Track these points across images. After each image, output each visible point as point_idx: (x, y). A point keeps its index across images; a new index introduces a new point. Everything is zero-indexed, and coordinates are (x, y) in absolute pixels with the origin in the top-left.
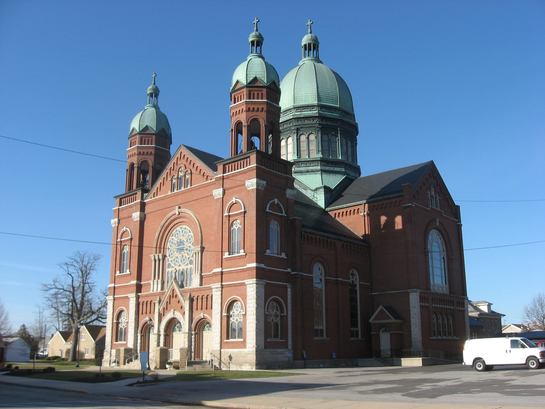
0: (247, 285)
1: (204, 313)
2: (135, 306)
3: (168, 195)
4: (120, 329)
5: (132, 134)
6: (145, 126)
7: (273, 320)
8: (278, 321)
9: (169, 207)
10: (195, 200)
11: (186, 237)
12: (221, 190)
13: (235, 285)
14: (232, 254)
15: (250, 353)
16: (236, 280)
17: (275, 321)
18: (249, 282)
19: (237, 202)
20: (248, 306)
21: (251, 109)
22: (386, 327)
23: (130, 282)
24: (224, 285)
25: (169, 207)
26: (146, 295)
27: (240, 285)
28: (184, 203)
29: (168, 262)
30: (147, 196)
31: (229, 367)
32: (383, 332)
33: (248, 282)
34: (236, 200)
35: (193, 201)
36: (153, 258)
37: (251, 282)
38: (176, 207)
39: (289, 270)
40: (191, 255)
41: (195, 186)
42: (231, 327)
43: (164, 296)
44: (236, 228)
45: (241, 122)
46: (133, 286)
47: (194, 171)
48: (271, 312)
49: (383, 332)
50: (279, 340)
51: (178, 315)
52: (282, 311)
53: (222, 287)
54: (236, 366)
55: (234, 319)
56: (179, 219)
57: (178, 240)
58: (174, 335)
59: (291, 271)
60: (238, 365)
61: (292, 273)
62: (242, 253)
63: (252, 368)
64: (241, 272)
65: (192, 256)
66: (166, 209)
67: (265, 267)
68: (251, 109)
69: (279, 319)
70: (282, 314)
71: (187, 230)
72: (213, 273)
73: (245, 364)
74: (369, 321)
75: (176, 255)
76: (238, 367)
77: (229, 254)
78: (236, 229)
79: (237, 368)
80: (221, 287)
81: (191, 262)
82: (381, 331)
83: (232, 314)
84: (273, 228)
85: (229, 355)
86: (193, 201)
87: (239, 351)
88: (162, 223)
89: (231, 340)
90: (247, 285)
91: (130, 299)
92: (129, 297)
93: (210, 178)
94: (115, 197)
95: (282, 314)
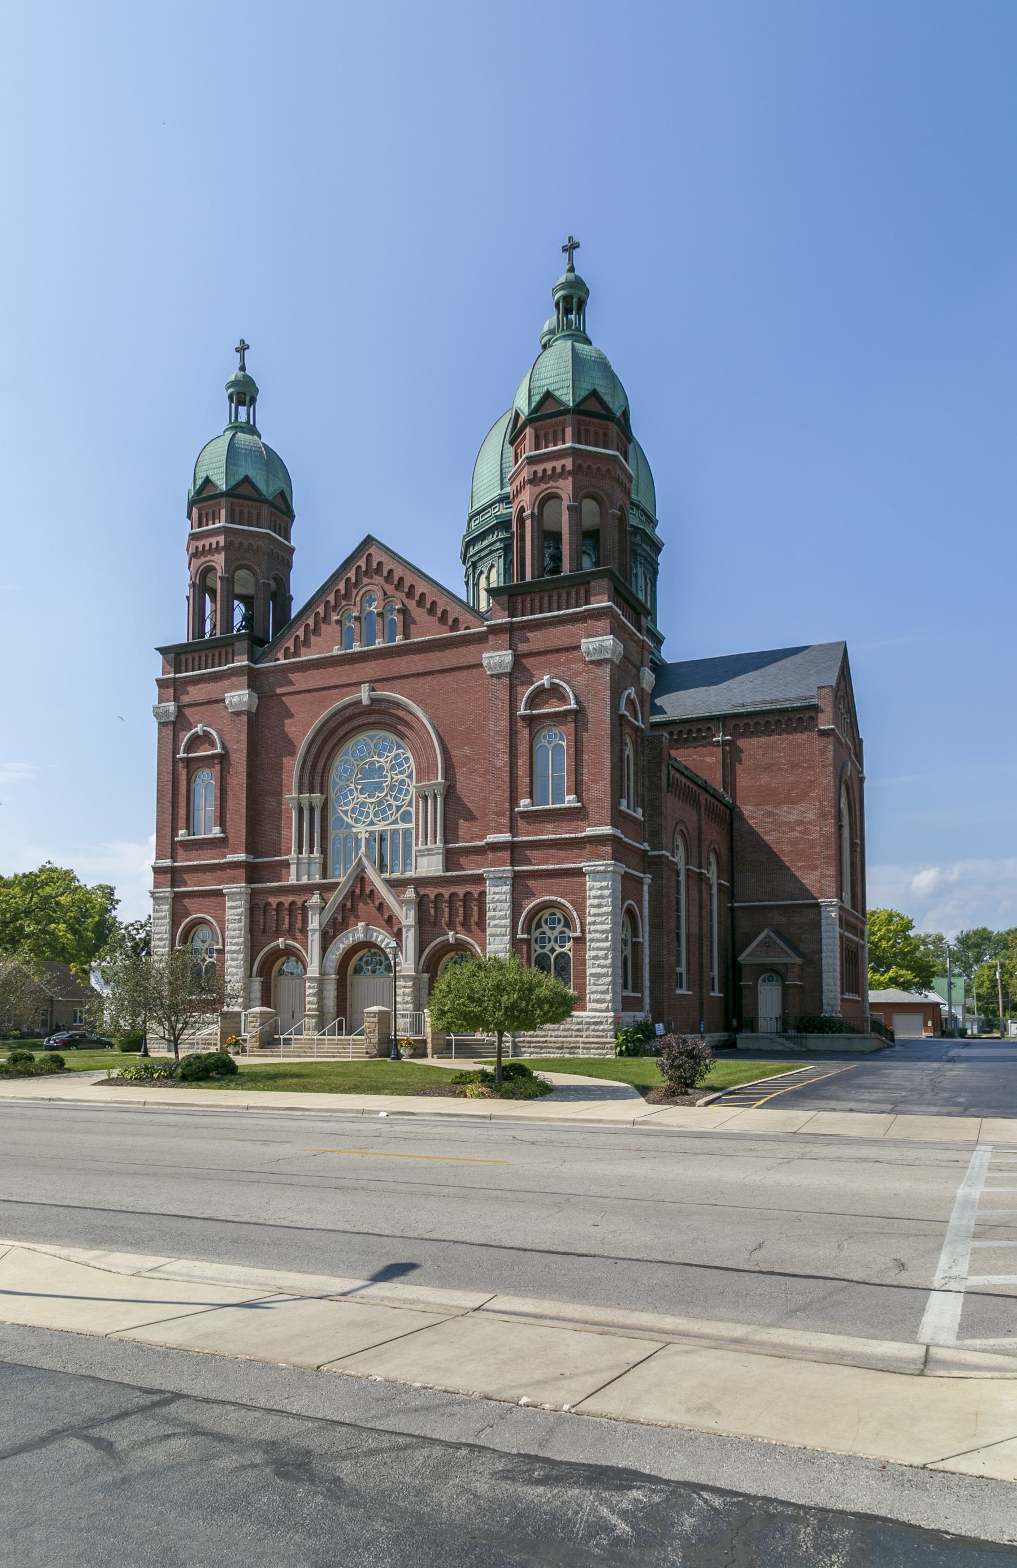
1: (457, 933)
6: (241, 477)
8: (570, 950)
11: (389, 759)
12: (506, 657)
14: (194, 835)
17: (559, 950)
19: (554, 686)
22: (776, 972)
32: (764, 981)
34: (205, 728)
39: (646, 846)
40: (407, 801)
41: (416, 640)
47: (411, 605)
48: (549, 933)
49: (764, 981)
51: (383, 939)
59: (648, 848)
61: (650, 853)
62: (216, 832)
65: (410, 805)
67: (622, 836)
70: (634, 940)
71: (392, 742)
72: (487, 844)
74: (739, 959)
75: (358, 798)
81: (406, 817)
82: (760, 980)
84: (548, 745)
93: (464, 626)
95: (634, 940)
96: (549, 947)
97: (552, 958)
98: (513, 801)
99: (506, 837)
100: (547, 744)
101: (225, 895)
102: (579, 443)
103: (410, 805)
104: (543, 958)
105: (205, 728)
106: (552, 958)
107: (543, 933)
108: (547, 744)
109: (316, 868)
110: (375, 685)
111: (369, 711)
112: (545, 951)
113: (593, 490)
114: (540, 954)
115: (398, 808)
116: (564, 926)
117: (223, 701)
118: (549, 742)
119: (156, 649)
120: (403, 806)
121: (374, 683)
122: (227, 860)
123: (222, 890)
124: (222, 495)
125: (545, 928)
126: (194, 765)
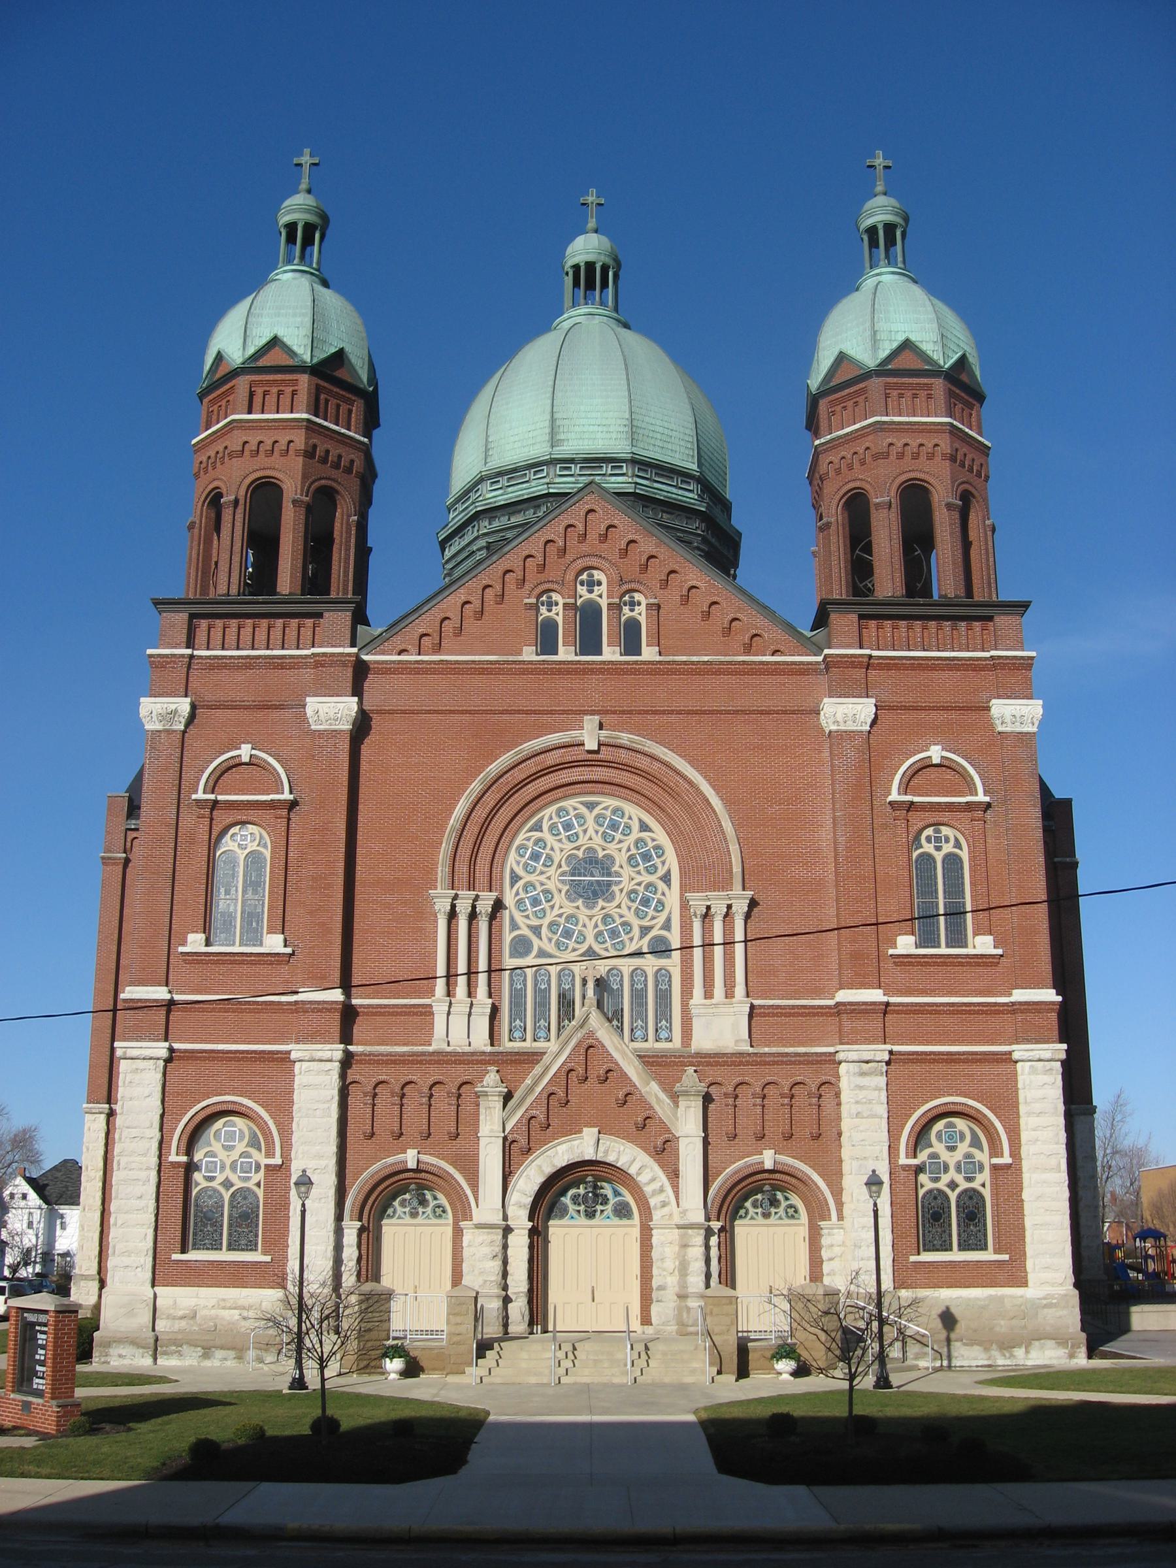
0: (1016, 1062)
2: (337, 1098)
3: (521, 662)
4: (196, 1196)
5: (260, 363)
6: (333, 350)
7: (953, 1185)
8: (983, 1185)
9: (527, 712)
10: (689, 712)
13: (951, 1058)
15: (1054, 1301)
16: (953, 1043)
17: (964, 1185)
18: (1035, 1052)
19: (254, 761)
20: (1025, 1136)
21: (319, 452)
23: (1010, 995)
24: (179, 1050)
25: (527, 712)
26: (403, 1054)
27: (979, 1061)
28: (623, 712)
29: (512, 931)
30: (378, 642)
31: (949, 1358)
33: (1031, 1053)
34: (254, 752)
35: (679, 713)
36: (442, 906)
37: (1047, 1055)
38: (587, 718)
42: (197, 1205)
43: (538, 1069)
44: (242, 855)
45: (279, 487)
46: (329, 1010)
48: (222, 1155)
50: (988, 1256)
52: (995, 1151)
53: (347, 1061)
54: (987, 1350)
55: (249, 1178)
56: (627, 774)
57: (578, 848)
58: (384, 1229)
60: (994, 1346)
63: (1072, 1356)
64: (983, 1012)
66: (505, 717)
68: (319, 452)
69: (985, 1176)
73: (1037, 1343)
76: (995, 1353)
77: (208, 943)
78: (242, 857)
79: (989, 1359)
80: (340, 1062)
83: (201, 1160)
85: (944, 1308)
86: (679, 713)
87: (990, 1297)
88: (494, 768)
89: (192, 1255)
90: (1016, 1062)
91: (297, 1065)
92: (1015, 1056)
94: (157, 603)
96: (945, 1179)
97: (953, 1196)
98: (172, 937)
99: (160, 993)
100: (236, 849)
101: (840, 1063)
102: (316, 415)
103: (667, 926)
104: (971, 1198)
105: (254, 752)
106: (953, 1196)
107: (934, 1156)
108: (236, 849)
109: (481, 1025)
110: (607, 719)
111: (592, 760)
112: (941, 1185)
113: (323, 482)
114: (966, 1191)
115: (645, 930)
116: (971, 1146)
117: (988, 709)
118: (938, 849)
119: (1030, 602)
120: (652, 927)
121: (607, 715)
122: (1012, 999)
123: (289, 1052)
124: (301, 369)
125: (939, 1147)
126: (219, 815)
